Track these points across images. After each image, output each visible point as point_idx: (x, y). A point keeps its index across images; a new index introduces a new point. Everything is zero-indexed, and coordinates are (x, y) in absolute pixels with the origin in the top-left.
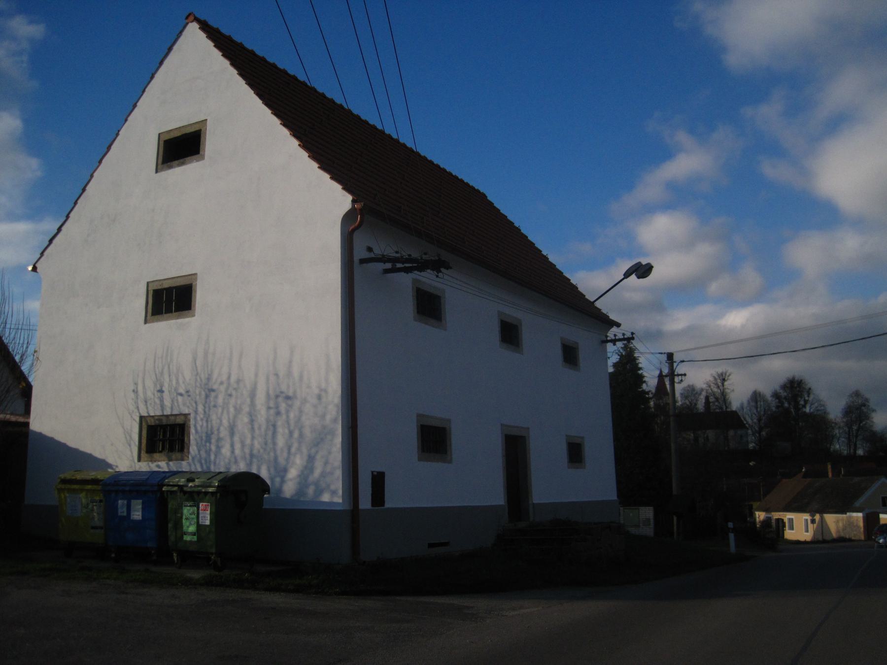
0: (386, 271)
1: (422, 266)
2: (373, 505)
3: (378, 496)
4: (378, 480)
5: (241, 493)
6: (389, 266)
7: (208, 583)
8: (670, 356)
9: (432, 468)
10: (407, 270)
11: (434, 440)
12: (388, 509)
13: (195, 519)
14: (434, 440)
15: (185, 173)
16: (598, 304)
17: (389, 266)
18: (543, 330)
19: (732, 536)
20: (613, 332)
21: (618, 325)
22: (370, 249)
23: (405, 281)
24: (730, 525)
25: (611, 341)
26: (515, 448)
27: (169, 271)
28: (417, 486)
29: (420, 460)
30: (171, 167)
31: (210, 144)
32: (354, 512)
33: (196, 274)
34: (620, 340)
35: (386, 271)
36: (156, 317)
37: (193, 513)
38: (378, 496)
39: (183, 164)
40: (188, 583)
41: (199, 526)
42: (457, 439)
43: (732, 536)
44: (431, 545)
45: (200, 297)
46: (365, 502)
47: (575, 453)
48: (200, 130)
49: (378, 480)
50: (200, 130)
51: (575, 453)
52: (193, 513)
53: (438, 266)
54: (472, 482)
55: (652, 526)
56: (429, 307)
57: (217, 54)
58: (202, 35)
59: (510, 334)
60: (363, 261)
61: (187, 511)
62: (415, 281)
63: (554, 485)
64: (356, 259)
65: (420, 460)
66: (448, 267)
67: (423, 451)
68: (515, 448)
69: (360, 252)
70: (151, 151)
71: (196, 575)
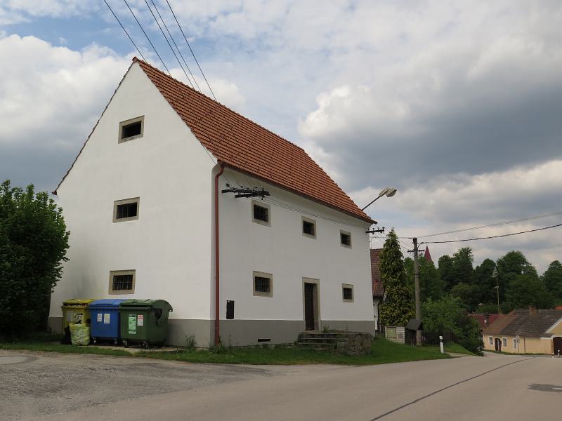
0: (237, 196)
1: (254, 194)
2: (227, 318)
3: (230, 314)
4: (230, 305)
5: (157, 311)
6: (237, 194)
7: (137, 356)
8: (415, 240)
9: (262, 299)
10: (247, 196)
11: (262, 285)
12: (236, 320)
13: (135, 323)
14: (262, 285)
15: (134, 143)
16: (364, 211)
17: (237, 194)
18: (328, 229)
19: (442, 344)
20: (373, 227)
21: (376, 223)
22: (228, 185)
23: (248, 203)
24: (441, 338)
25: (371, 232)
26: (310, 290)
27: (126, 196)
28: (252, 309)
29: (254, 295)
30: (126, 141)
31: (146, 128)
32: (217, 322)
33: (139, 198)
34: (376, 231)
35: (237, 196)
36: (118, 220)
37: (134, 320)
38: (230, 314)
39: (132, 139)
40: (130, 355)
41: (137, 326)
42: (276, 285)
43: (442, 344)
44: (259, 340)
45: (141, 210)
46: (223, 316)
47: (348, 293)
48: (140, 122)
49: (230, 305)
50: (140, 122)
51: (348, 293)
52: (134, 320)
53: (263, 194)
54: (285, 307)
55: (404, 337)
56: (261, 214)
57: (149, 81)
58: (141, 70)
59: (308, 228)
60: (223, 192)
61: (131, 319)
62: (253, 201)
63: (332, 311)
64: (220, 191)
65: (254, 295)
66: (268, 194)
67: (256, 290)
68: (310, 290)
69: (222, 187)
70: (116, 132)
71: (133, 351)
